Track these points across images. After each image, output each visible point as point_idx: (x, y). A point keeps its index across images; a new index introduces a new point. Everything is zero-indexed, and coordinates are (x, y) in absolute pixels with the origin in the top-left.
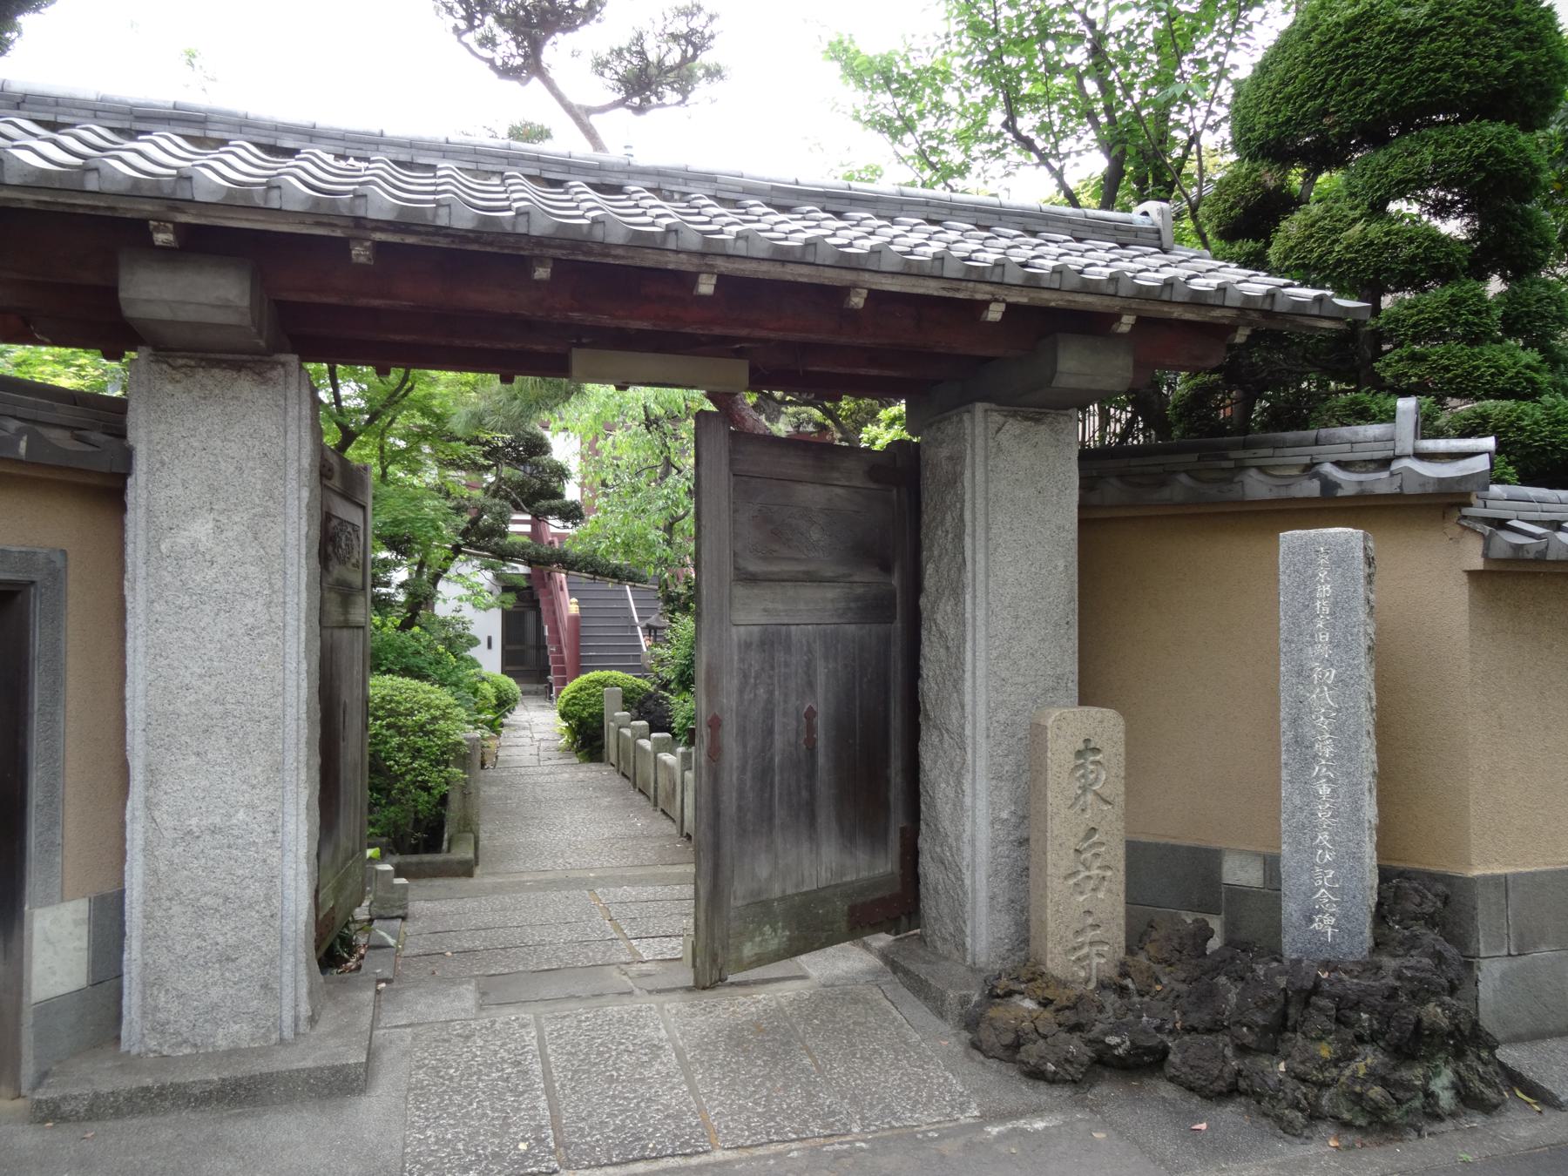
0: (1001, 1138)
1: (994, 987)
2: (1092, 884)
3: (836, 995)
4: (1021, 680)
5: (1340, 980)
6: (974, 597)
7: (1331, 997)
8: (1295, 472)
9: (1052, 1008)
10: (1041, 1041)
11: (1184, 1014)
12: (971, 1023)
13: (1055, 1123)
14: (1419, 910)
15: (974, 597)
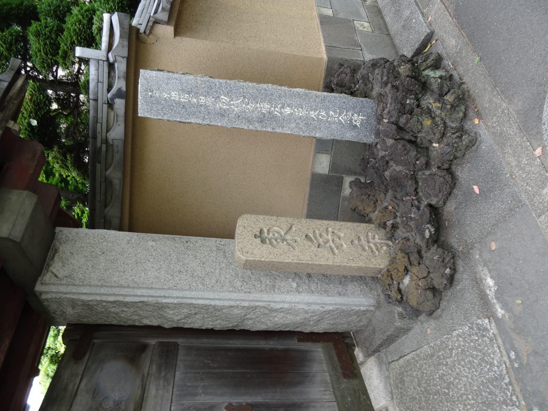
0: (505, 306)
1: (397, 300)
2: (337, 240)
4: (217, 271)
5: (389, 112)
6: (165, 297)
7: (399, 117)
8: (112, 114)
9: (409, 267)
10: (431, 275)
11: (407, 194)
12: (416, 313)
13: (486, 271)
14: (349, 75)
15: (165, 297)
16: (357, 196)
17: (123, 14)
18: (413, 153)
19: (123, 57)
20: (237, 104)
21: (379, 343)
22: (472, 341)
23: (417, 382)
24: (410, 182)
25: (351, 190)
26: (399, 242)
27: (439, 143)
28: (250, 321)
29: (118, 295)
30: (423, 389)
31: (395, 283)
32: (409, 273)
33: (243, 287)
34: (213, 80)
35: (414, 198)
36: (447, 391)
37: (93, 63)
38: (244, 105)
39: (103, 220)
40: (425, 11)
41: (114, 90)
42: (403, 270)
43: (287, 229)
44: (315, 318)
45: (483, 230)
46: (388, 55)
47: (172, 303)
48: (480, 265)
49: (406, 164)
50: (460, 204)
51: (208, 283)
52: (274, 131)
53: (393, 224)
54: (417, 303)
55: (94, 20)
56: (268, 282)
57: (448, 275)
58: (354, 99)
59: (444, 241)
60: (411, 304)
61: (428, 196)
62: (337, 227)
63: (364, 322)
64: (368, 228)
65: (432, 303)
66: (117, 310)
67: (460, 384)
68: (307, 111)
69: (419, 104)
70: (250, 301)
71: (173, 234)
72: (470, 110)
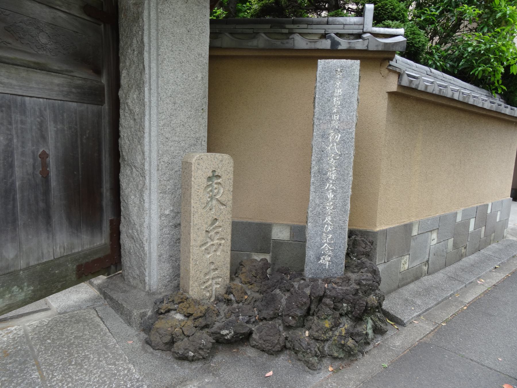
1: (159, 309)
2: (214, 248)
3: (71, 317)
4: (177, 139)
5: (334, 288)
6: (150, 89)
7: (330, 297)
8: (316, 38)
9: (192, 318)
10: (186, 339)
11: (260, 311)
14: (364, 250)
15: (150, 89)
16: (255, 266)
17: (405, 44)
18: (299, 313)
19: (367, 46)
20: (333, 147)
21: (114, 297)
22: (125, 382)
23: (79, 335)
24: (271, 313)
25: (259, 260)
26: (215, 307)
27: (309, 336)
28: (129, 172)
29: (150, 46)
30: (72, 341)
31: (176, 306)
32: (186, 318)
33: (162, 163)
34: (354, 126)
35: (257, 318)
36: (73, 363)
37: (358, 21)
38: (333, 155)
39: (218, 32)
40: (422, 317)
41: (337, 39)
42: (189, 312)
43: (221, 201)
44: (136, 234)
45: (232, 383)
46: (383, 287)
47: (144, 96)
48: (199, 384)
49: (289, 307)
50: (254, 361)
51: (165, 130)
52: (311, 184)
53: (231, 300)
54: (158, 328)
55: (396, 22)
56: (169, 187)
57: (187, 354)
58: (343, 256)
59: (218, 349)
60: (156, 322)
61: (260, 330)
62: (225, 249)
63: (133, 282)
64: (225, 278)
65: (159, 343)
66: (135, 46)
67: (82, 375)
68: (331, 213)
69: (343, 316)
70: (150, 171)
71: (209, 96)
72: (340, 362)
